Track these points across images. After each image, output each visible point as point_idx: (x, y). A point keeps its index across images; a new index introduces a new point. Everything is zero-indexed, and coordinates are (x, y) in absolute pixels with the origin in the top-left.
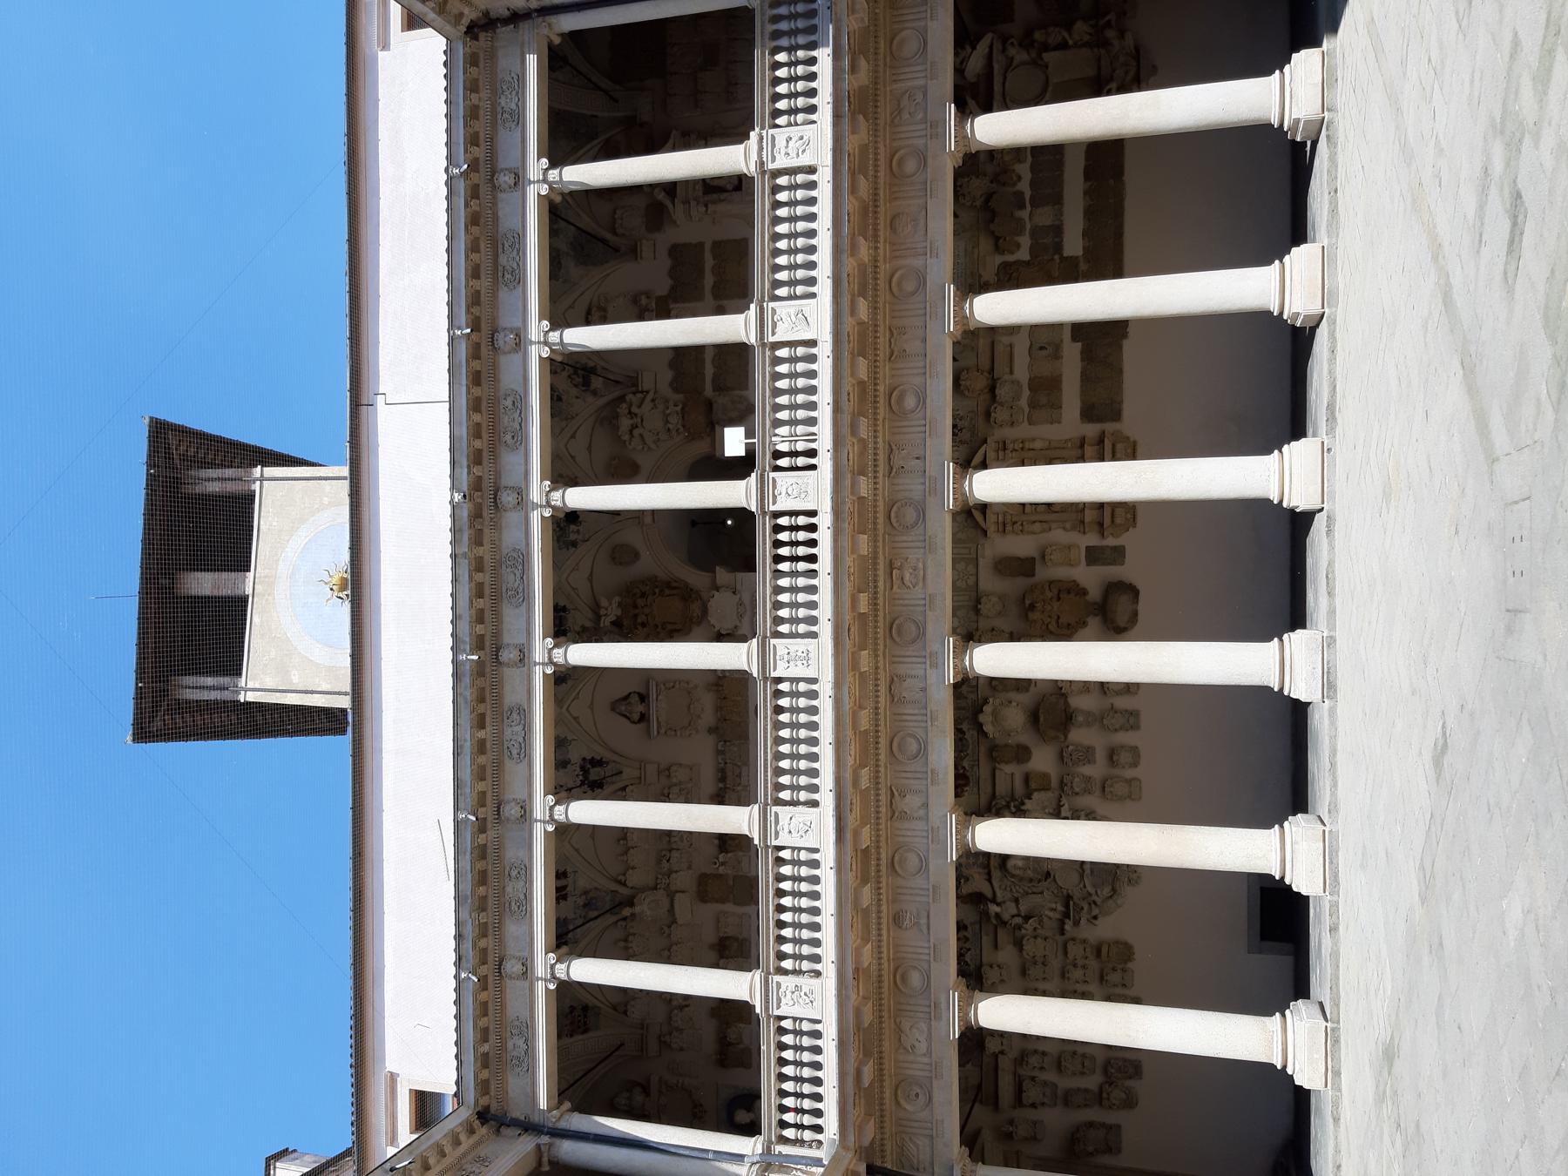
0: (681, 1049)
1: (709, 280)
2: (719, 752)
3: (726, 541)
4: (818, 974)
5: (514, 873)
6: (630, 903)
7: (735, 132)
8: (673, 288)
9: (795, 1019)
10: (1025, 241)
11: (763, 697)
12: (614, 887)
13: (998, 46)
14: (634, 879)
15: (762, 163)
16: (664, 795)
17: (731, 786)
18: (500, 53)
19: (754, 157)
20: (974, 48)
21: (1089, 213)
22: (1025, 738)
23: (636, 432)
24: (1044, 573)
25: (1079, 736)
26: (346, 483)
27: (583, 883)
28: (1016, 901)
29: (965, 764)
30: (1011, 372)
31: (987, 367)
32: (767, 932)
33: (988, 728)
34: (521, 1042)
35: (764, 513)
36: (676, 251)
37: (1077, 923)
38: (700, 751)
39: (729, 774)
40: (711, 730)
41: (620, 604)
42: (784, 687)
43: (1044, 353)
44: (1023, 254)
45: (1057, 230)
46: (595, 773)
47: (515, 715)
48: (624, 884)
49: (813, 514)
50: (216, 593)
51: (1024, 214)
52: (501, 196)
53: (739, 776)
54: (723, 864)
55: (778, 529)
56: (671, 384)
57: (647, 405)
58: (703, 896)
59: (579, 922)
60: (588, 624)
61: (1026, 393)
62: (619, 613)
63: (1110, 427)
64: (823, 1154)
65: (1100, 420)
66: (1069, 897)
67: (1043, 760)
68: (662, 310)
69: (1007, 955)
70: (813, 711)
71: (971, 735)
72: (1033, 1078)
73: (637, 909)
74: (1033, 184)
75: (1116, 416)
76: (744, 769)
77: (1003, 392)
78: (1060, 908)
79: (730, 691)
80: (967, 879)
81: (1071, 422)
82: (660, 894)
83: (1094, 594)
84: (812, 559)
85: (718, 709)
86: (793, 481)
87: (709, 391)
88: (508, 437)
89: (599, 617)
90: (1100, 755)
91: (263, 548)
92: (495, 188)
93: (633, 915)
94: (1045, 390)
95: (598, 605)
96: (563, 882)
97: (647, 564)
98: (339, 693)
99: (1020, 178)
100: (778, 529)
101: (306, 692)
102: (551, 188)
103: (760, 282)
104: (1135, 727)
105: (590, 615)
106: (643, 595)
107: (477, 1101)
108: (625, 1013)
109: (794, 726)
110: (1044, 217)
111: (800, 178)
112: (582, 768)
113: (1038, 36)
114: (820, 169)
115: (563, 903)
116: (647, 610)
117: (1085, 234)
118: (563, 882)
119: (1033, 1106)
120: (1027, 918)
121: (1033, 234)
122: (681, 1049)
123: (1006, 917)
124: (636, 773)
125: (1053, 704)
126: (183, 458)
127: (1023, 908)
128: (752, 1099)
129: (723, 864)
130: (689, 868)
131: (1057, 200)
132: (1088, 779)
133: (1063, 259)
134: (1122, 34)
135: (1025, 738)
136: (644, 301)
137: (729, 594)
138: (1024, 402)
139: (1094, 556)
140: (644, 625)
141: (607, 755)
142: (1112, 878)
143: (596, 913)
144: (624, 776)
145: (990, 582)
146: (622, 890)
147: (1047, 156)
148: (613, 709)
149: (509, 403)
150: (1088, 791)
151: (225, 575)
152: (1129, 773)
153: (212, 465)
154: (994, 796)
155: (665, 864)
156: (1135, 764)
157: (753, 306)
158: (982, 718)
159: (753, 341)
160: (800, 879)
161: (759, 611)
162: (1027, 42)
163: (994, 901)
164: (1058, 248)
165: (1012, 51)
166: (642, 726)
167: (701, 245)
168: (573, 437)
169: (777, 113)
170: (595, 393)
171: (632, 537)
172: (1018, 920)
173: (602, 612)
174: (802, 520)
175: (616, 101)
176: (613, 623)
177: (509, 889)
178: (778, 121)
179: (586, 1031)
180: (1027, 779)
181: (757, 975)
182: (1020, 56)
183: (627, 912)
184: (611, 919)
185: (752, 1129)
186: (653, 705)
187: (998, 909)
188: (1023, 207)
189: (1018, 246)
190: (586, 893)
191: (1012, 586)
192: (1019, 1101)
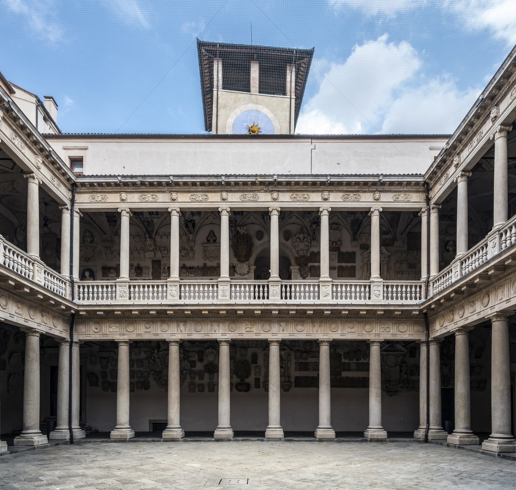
0: (106, 254)
1: (344, 265)
2: (198, 267)
3: (160, 270)
4: (130, 299)
5: (154, 196)
6: (150, 237)
7: (382, 275)
8: (342, 253)
9: (115, 291)
10: (347, 361)
11: (214, 282)
12: (155, 231)
13: (403, 353)
14: (158, 238)
15: (373, 282)
16: (182, 249)
17: (186, 270)
18: (418, 194)
19: (375, 280)
20: (403, 346)
21: (353, 379)
22: (205, 362)
23: (298, 239)
24: (253, 366)
25: (207, 376)
26: (288, 133)
27: (155, 220)
28: (159, 358)
29: (197, 343)
30: (310, 357)
31: (312, 350)
32: (141, 282)
33: (208, 351)
34: (100, 199)
35: (167, 282)
36: (353, 254)
37: (153, 374)
38: (198, 262)
39: (192, 270)
40: (205, 264)
41: (244, 233)
42: (215, 289)
43: (315, 366)
44: (343, 360)
45: (349, 370)
46: (190, 224)
47: (206, 197)
48: (156, 234)
49: (268, 298)
50: (251, 78)
51: (355, 361)
52: (372, 194)
53: (191, 273)
54: (164, 268)
55: (263, 286)
56: (313, 252)
57: (306, 243)
58: (153, 262)
59: (142, 219)
60: (238, 222)
61: (304, 361)
62: (241, 233)
63: (293, 385)
64: (76, 301)
65: (295, 381)
66: (161, 373)
67: (199, 366)
68: (332, 249)
69: (143, 355)
70: (397, 298)
71: (206, 345)
72: (108, 362)
73: (148, 239)
74: (363, 363)
75: (296, 386)
76: (193, 275)
77: (305, 355)
78: (157, 370)
79: (215, 271)
80: (164, 344)
81: (294, 373)
82: (153, 247)
83: (247, 380)
84: (259, 298)
85: (212, 267)
86: (278, 292)
87: (310, 264)
88: (295, 196)
89: (240, 226)
90: (201, 382)
91: (267, 98)
92: (374, 192)
93: (146, 238)
94: (303, 366)
95: (243, 226)
96: (155, 214)
97: (257, 243)
98: (217, 129)
99: (365, 359)
100: (263, 286)
101: (217, 116)
102: (373, 212)
103: (338, 282)
104: (209, 391)
105: (241, 223)
106: (247, 241)
107: (78, 182)
108: (116, 235)
109: (360, 292)
110: (353, 366)
111: (367, 295)
112: (192, 220)
113: (405, 364)
114: (268, 300)
115: (148, 213)
116: (242, 243)
117: (347, 377)
118: (155, 214)
119: (101, 362)
120: (154, 361)
121: (348, 363)
122: (106, 254)
123: (154, 355)
124: (191, 239)
125: (213, 369)
126: (299, 65)
127: (157, 360)
128: (93, 277)
129: (164, 268)
130: (162, 257)
131: (358, 370)
132: (194, 378)
133: (341, 371)
134: (401, 387)
135: (205, 362)
136: (339, 243)
137: (247, 270)
138: (301, 361)
139: (257, 380)
140: (238, 241)
141: (196, 229)
142: (165, 384)
143: (146, 225)
144: (190, 235)
145: (250, 351)
146: (154, 234)
147: (366, 367)
148: (211, 231)
149: (306, 196)
150: (191, 378)
151: (258, 82)
152: (196, 389)
153: (297, 77)
154: (188, 352)
155: (163, 249)
156: (199, 391)
157: (331, 279)
158: (211, 348)
159: (320, 279)
160: (88, 294)
161: (106, 281)
162: (403, 362)
163: (158, 351)
164: (344, 370)
165: (401, 357)
166: (206, 241)
167: (355, 262)
168: (298, 218)
169: (387, 287)
170: (311, 226)
171: (265, 239)
172: (153, 358)
173: (242, 228)
174: (266, 294)
175: (402, 234)
176: (238, 231)
177: (149, 195)
178: (334, 287)
179: (108, 221)
180: (194, 361)
181: (128, 280)
182: (399, 360)
183: (147, 236)
184: (144, 230)
185: (82, 277)
186: (212, 245)
187: (156, 352)
188: (357, 360)
189: (346, 359)
190: (152, 222)
191: (249, 358)
192: (101, 358)
